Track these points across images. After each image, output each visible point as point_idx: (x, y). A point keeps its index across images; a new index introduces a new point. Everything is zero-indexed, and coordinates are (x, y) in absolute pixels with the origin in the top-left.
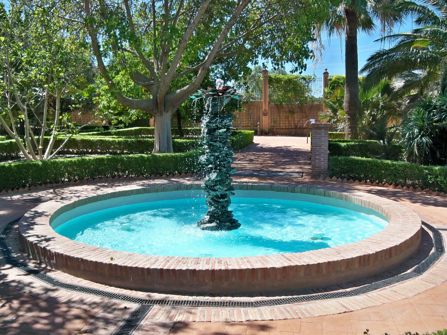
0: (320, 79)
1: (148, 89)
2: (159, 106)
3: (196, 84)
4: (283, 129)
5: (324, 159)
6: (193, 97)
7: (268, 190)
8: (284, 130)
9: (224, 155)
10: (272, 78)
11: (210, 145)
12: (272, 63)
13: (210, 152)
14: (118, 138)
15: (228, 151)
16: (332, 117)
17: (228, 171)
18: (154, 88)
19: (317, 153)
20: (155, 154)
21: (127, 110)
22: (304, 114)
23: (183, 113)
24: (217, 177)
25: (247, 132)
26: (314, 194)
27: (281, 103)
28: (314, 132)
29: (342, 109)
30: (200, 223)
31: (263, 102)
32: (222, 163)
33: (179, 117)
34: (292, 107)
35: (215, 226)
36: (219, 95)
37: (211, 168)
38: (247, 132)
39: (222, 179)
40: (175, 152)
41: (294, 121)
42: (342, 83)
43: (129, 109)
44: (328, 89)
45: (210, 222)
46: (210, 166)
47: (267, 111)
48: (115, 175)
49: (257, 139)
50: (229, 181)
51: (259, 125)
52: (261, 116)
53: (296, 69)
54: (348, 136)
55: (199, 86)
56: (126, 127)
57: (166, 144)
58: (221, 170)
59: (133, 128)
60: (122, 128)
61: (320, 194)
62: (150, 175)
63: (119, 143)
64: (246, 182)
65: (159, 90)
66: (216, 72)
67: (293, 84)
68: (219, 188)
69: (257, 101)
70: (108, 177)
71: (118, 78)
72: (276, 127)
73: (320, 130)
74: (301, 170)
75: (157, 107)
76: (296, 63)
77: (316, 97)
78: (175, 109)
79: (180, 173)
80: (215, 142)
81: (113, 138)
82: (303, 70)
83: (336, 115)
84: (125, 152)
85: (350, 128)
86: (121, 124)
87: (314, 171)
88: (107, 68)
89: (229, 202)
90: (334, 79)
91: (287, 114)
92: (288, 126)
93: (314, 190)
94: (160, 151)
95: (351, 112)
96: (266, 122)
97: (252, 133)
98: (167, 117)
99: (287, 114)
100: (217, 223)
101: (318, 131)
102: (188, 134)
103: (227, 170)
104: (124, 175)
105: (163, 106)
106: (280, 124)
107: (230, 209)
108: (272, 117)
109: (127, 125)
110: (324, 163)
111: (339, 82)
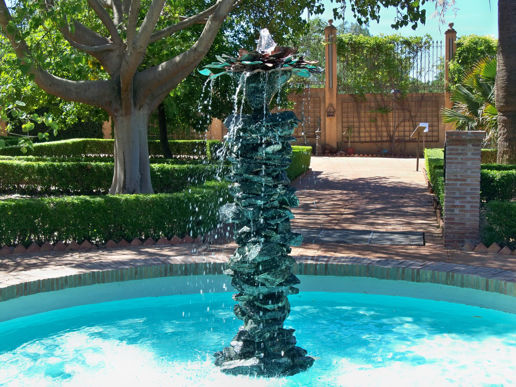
0: (439, 44)
1: (101, 58)
2: (123, 96)
3: (200, 50)
4: (365, 142)
5: (471, 207)
6: (205, 72)
7: (360, 275)
8: (368, 144)
9: (276, 203)
10: (344, 42)
12: (353, 10)
13: (245, 198)
14: (38, 160)
15: (285, 194)
16: (469, 119)
17: (286, 241)
18: (114, 56)
19: (457, 195)
20: (117, 196)
21: (57, 105)
22: (407, 114)
23: (173, 110)
24: (261, 254)
26: (462, 285)
27: (361, 91)
28: (451, 150)
29: (489, 101)
30: (221, 357)
31: (327, 89)
33: (162, 118)
37: (248, 235)
39: (273, 260)
40: (156, 193)
41: (387, 126)
42: (482, 52)
43: (60, 101)
44: (455, 62)
45: (245, 355)
46: (246, 229)
47: (335, 106)
48: (30, 242)
49: (317, 164)
50: (287, 263)
51: (319, 134)
53: (403, 23)
54: (502, 157)
55: (203, 58)
56: (52, 138)
57: (138, 174)
58: (270, 237)
59: (70, 141)
60: (44, 140)
61: (477, 286)
62: (106, 241)
63: (41, 171)
64: (313, 258)
65: (124, 63)
66: (236, 29)
67: (386, 55)
68: (267, 280)
70: (15, 245)
71: (38, 35)
72: (352, 139)
73: (463, 145)
74: (409, 229)
75: (119, 96)
76: (403, 8)
77: (423, 81)
78: (156, 103)
80: (257, 173)
81: (28, 160)
82: (419, 22)
83: (477, 115)
84: (53, 188)
85: (506, 140)
86: (43, 132)
87: (450, 231)
88: (13, 13)
89: (285, 310)
90: (466, 43)
91: (374, 114)
92: (376, 137)
93: (462, 277)
94: (125, 189)
95: (510, 109)
96: (332, 130)
97: (308, 151)
98: (140, 120)
99: (374, 114)
101: (460, 148)
103: (284, 239)
104: (49, 240)
105: (131, 95)
106: (359, 132)
109: (55, 133)
110: (473, 216)
111: (476, 50)
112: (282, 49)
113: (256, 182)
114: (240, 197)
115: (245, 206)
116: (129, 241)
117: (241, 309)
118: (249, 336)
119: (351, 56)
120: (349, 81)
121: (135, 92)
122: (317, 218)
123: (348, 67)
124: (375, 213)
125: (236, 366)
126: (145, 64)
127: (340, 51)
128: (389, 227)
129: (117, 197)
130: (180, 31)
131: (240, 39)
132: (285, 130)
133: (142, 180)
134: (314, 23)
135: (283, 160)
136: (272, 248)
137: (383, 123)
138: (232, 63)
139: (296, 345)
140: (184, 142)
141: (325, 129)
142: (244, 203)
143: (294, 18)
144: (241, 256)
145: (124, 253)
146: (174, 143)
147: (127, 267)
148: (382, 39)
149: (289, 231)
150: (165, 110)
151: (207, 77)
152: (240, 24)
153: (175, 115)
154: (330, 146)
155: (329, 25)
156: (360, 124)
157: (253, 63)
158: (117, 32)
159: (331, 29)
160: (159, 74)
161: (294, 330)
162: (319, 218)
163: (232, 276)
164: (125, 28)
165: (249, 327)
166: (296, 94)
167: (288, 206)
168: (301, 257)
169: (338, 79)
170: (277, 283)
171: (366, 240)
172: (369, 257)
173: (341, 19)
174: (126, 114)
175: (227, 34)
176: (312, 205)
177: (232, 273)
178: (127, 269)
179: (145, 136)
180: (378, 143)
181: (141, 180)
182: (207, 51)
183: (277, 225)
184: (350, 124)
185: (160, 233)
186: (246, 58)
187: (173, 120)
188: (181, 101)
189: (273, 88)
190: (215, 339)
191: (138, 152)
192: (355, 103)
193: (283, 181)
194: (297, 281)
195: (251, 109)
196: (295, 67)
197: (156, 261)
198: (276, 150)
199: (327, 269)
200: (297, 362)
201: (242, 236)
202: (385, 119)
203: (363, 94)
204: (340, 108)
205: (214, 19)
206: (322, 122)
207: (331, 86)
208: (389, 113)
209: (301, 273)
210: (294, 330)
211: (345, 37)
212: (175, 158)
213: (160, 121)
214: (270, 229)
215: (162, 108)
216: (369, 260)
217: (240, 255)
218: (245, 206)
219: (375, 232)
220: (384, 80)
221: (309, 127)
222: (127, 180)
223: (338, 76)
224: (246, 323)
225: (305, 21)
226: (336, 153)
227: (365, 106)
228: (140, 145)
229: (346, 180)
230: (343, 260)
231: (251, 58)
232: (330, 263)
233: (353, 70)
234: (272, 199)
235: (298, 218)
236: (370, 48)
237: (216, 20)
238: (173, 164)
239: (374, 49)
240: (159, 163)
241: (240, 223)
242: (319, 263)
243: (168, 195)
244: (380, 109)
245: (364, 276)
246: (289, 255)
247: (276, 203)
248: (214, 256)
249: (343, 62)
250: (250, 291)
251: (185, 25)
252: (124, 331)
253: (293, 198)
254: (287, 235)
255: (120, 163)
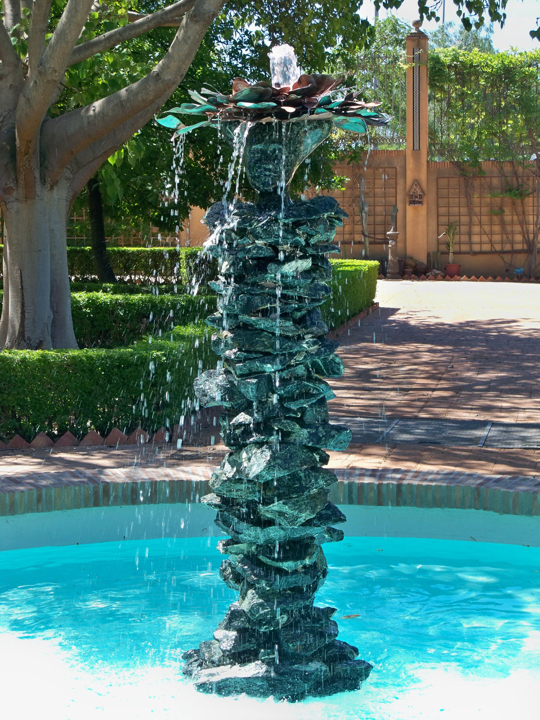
2: (20, 164)
3: (167, 77)
4: (481, 253)
10: (443, 64)
11: (241, 330)
15: (318, 353)
17: (318, 442)
23: (114, 190)
24: (270, 467)
25: (352, 264)
27: (475, 155)
31: (409, 153)
32: (293, 406)
33: (94, 202)
34: (515, 173)
35: (263, 678)
36: (283, 115)
38: (352, 264)
39: (294, 477)
40: (81, 347)
41: (523, 223)
45: (239, 656)
46: (242, 418)
47: (424, 184)
49: (389, 294)
50: (321, 482)
51: (394, 238)
52: (400, 206)
64: (373, 473)
65: (22, 100)
66: (236, 37)
68: (281, 514)
69: (381, 147)
72: (457, 248)
78: (85, 176)
79: (104, 431)
80: (265, 313)
89: (317, 572)
92: (502, 243)
96: (417, 231)
97: (371, 269)
99: (498, 200)
100: (270, 663)
102: (127, 270)
105: (35, 163)
106: (470, 234)
107: (320, 603)
108: (443, 210)
112: (313, 79)
113: (262, 330)
114: (233, 357)
115: (240, 376)
116: (28, 438)
117: (233, 568)
118: (249, 621)
119: (456, 89)
120: (452, 137)
121: (43, 157)
122: (382, 396)
123: (449, 111)
124: (498, 387)
125: (223, 676)
126: (63, 102)
127: (434, 80)
128: (521, 415)
129: (7, 354)
130: (130, 40)
131: (243, 58)
132: (317, 232)
133: (56, 324)
134: (385, 26)
135: (316, 289)
136: (292, 454)
137: (515, 218)
138: (219, 105)
139: (337, 638)
140: (138, 251)
141: (405, 227)
142: (241, 369)
143: (345, 16)
144: (235, 469)
145: (16, 461)
146: (119, 252)
147: (22, 488)
148: (516, 58)
149: (325, 423)
150: (101, 191)
151: (173, 131)
152: (243, 27)
153: (118, 202)
154: (415, 261)
155: (414, 31)
156: (471, 219)
157: (260, 106)
158: (10, 42)
159: (419, 38)
160: (89, 123)
161: (333, 610)
162: (389, 397)
163: (216, 506)
164: (26, 36)
165: (248, 602)
166: (349, 163)
167: (324, 374)
168: (351, 471)
169: (430, 133)
170: (302, 520)
171: (474, 441)
172: (480, 472)
173: (433, 19)
174: (51, 190)
175: (219, 47)
176: (377, 373)
177: (217, 501)
178: (22, 492)
179: (62, 237)
180: (504, 256)
181: (53, 322)
182: (179, 81)
183: (303, 410)
184: (452, 219)
185: (88, 424)
186: (246, 95)
187: (117, 209)
188: (134, 173)
189: (295, 152)
190: (182, 626)
191: (49, 270)
192: (462, 179)
193: (314, 328)
194: (340, 518)
195: (254, 192)
196: (338, 113)
197: (77, 477)
198: (300, 270)
199: (401, 495)
200: (342, 672)
201: (237, 431)
202: (520, 209)
203: (477, 162)
204: (434, 189)
205: (193, 18)
206: (400, 215)
207: (416, 147)
208: (527, 199)
209: (351, 502)
210: (333, 610)
211: (444, 53)
212: (121, 280)
213: (92, 212)
214: (289, 418)
215: (95, 186)
216: (480, 477)
217: (233, 467)
218: (240, 376)
219: (494, 424)
220: (517, 134)
221: (374, 224)
222: (26, 322)
223: (430, 128)
224: (244, 596)
225: (366, 23)
226: (425, 273)
227: (481, 185)
228: (52, 256)
229: (443, 324)
230: (431, 477)
231: (256, 96)
232: (405, 482)
233: (458, 116)
234: (293, 362)
235: (345, 397)
236: (491, 74)
237: (197, 22)
238: (115, 293)
239: (500, 76)
240: (90, 290)
241: (232, 407)
242: (385, 482)
243: (103, 352)
244: (510, 190)
245: (470, 507)
246: (324, 467)
247: (301, 370)
248: (378, 465)
249: (440, 101)
250: (250, 535)
251: (138, 31)
252: (16, 611)
253: (333, 360)
254: (321, 429)
255: (13, 292)
